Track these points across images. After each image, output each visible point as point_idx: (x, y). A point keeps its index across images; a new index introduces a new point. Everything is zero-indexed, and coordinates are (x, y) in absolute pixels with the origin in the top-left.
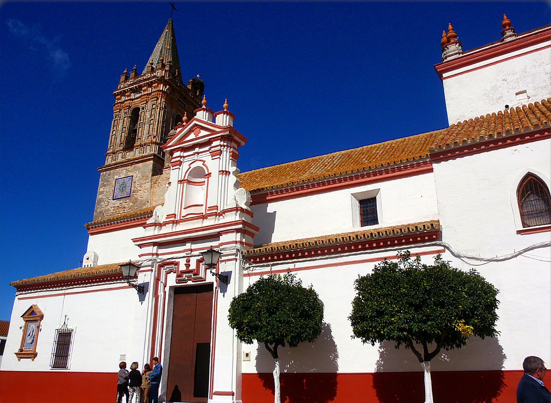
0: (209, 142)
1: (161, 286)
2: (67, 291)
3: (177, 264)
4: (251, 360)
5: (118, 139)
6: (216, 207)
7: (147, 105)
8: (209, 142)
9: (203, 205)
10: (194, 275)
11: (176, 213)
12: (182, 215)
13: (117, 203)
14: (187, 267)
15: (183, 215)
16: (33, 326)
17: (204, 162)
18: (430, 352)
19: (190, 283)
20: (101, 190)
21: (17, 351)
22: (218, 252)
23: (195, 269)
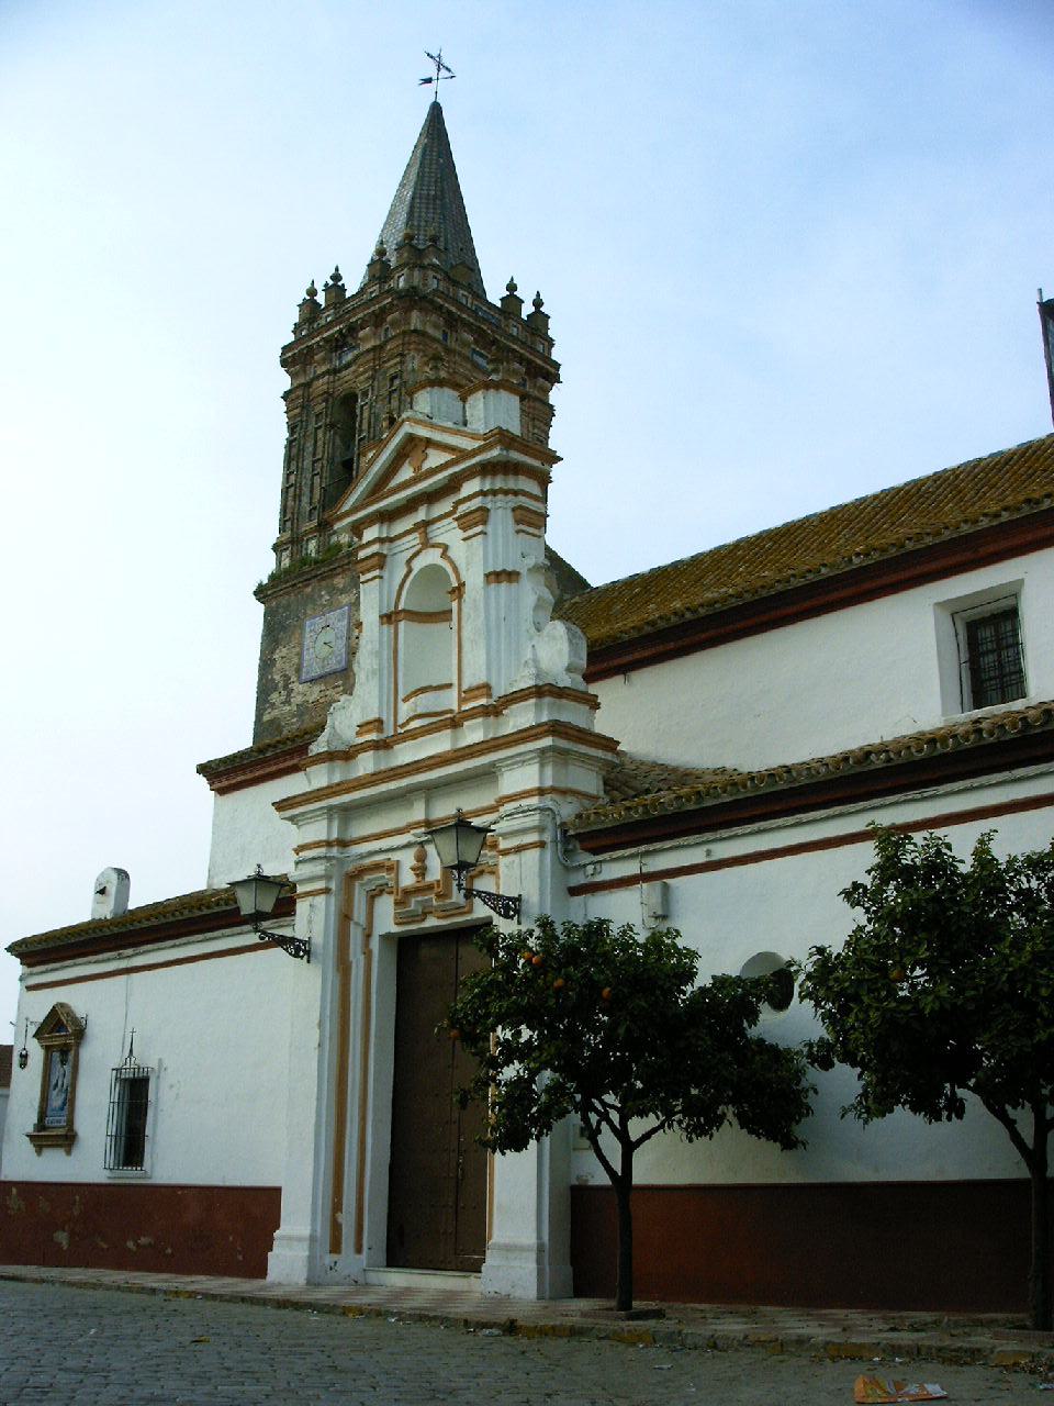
0: (453, 485)
1: (356, 935)
2: (723, 850)
3: (393, 868)
5: (305, 499)
6: (486, 688)
7: (376, 383)
8: (453, 485)
9: (449, 686)
10: (439, 896)
11: (384, 718)
12: (400, 722)
14: (417, 875)
17: (446, 548)
19: (432, 922)
23: (438, 881)
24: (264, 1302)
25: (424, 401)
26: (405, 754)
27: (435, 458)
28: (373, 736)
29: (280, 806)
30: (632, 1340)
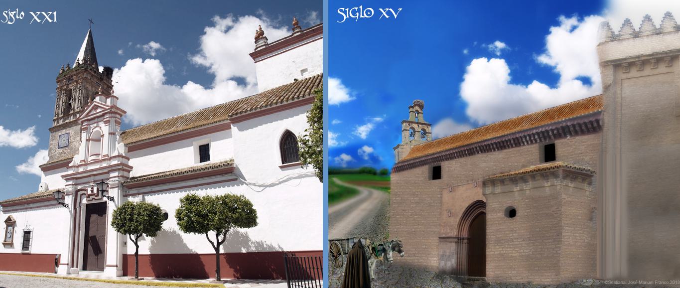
0: (103, 115)
3: (86, 190)
4: (329, 242)
5: (60, 110)
8: (103, 115)
9: (100, 154)
13: (61, 150)
15: (89, 160)
16: (10, 228)
17: (101, 127)
18: (220, 241)
20: (51, 142)
21: (3, 242)
22: (107, 183)
24: (58, 278)
25: (97, 99)
26: (90, 168)
27: (99, 110)
28: (83, 163)
29: (63, 177)
30: (137, 284)
